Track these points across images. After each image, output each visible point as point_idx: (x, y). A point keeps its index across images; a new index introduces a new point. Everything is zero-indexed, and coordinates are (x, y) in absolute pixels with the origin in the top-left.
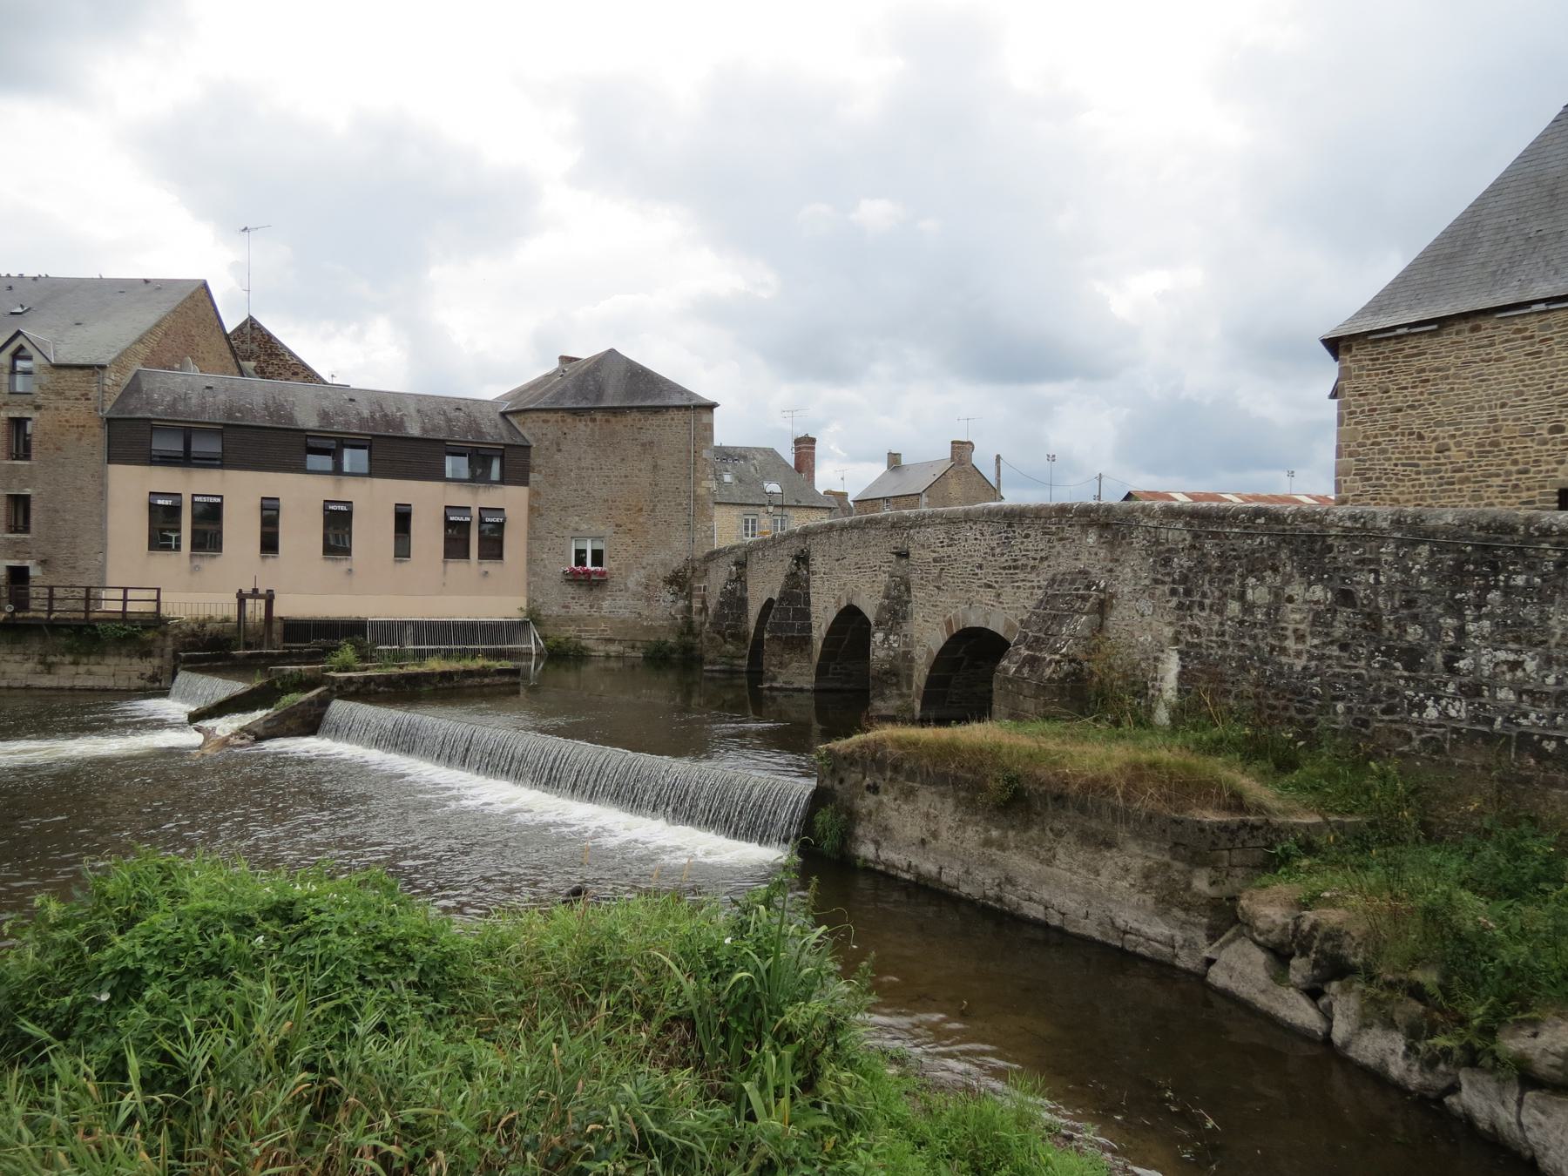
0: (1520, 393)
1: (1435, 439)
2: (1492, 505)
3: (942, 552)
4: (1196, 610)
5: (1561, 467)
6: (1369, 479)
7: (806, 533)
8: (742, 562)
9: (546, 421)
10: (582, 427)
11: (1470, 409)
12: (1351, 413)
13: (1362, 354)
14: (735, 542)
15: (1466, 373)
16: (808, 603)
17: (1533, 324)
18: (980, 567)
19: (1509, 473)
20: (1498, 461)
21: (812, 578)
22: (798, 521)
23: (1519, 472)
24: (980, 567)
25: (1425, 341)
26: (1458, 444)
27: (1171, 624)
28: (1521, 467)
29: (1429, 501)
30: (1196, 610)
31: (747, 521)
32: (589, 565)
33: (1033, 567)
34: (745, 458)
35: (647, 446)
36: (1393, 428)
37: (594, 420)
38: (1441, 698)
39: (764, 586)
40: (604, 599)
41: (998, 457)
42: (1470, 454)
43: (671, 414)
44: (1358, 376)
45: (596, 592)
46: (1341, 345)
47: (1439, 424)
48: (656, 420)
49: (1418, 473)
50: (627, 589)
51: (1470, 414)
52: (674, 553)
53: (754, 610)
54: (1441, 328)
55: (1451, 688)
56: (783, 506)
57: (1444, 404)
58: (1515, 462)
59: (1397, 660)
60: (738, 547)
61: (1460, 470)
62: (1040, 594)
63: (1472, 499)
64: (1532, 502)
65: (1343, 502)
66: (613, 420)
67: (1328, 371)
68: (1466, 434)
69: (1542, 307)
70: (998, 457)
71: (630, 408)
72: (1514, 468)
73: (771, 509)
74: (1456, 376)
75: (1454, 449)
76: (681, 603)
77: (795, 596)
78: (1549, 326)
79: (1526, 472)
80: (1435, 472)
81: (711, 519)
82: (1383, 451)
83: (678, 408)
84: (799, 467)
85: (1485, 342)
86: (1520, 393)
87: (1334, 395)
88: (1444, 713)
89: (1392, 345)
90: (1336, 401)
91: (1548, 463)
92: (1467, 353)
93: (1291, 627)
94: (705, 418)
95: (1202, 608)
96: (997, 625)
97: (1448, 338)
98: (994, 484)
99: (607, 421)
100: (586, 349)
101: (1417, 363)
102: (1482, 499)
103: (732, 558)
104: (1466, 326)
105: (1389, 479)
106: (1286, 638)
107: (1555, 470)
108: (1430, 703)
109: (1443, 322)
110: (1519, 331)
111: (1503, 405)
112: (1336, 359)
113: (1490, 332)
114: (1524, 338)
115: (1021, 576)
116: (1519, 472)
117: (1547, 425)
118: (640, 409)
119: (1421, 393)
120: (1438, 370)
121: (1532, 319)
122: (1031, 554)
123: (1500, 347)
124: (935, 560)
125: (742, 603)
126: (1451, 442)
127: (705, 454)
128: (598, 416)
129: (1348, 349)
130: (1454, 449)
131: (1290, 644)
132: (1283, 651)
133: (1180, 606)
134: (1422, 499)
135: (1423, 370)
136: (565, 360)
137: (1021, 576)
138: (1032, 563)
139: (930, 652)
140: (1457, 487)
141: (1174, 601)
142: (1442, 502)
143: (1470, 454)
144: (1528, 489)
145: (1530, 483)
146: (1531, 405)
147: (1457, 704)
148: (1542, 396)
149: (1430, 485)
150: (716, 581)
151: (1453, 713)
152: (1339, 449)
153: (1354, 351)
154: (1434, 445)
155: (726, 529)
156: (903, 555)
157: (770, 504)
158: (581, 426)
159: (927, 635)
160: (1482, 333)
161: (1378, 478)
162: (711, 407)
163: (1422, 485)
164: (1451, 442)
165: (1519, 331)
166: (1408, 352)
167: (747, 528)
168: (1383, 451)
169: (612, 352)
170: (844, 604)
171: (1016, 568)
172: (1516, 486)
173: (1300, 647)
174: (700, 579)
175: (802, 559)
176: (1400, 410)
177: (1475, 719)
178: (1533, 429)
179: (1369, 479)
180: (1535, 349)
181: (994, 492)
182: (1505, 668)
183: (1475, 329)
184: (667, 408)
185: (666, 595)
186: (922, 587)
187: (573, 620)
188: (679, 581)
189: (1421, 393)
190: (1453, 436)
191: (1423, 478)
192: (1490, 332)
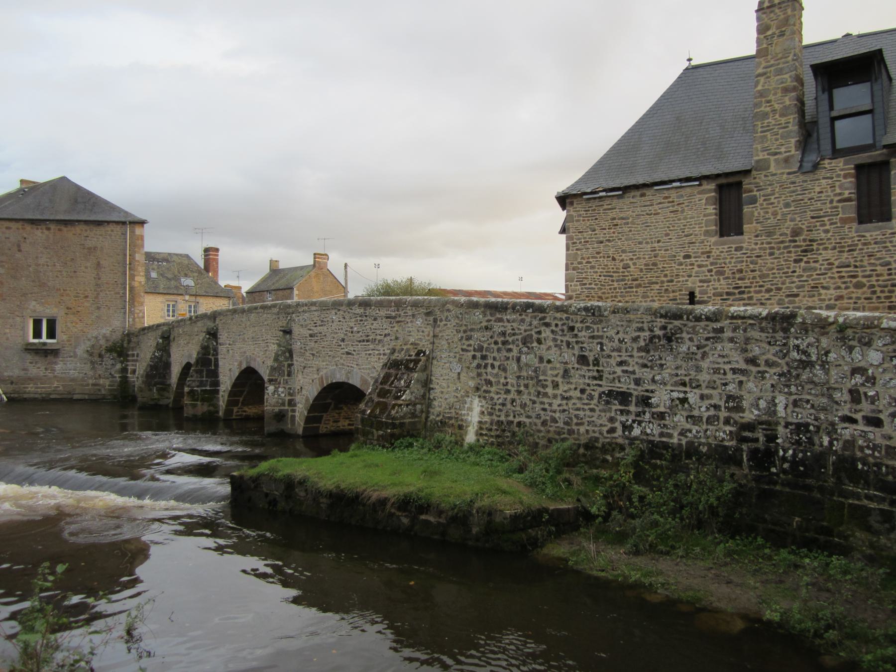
0: (667, 235)
1: (622, 260)
2: (654, 301)
3: (316, 330)
4: (489, 369)
5: (690, 279)
6: (585, 284)
7: (214, 316)
8: (166, 336)
9: (8, 228)
10: (39, 234)
11: (640, 243)
12: (574, 243)
13: (579, 207)
14: (162, 321)
15: (638, 221)
16: (217, 365)
17: (673, 195)
18: (343, 340)
19: (662, 282)
20: (656, 274)
21: (220, 347)
22: (208, 306)
23: (668, 281)
24: (343, 340)
25: (615, 201)
26: (634, 264)
27: (473, 378)
28: (669, 278)
29: (620, 298)
30: (489, 369)
31: (168, 306)
32: (44, 339)
33: (380, 341)
34: (167, 261)
35: (92, 250)
36: (598, 253)
37: (48, 229)
38: (642, 422)
39: (183, 353)
40: (56, 363)
41: (346, 265)
42: (641, 270)
43: (109, 228)
44: (578, 221)
45: (50, 358)
46: (568, 201)
47: (624, 251)
48: (101, 230)
49: (613, 281)
50: (75, 356)
51: (641, 246)
52: (111, 327)
53: (176, 370)
54: (624, 193)
55: (647, 416)
56: (196, 295)
57: (626, 240)
58: (666, 276)
59: (615, 399)
60: (164, 324)
61: (636, 280)
62: (384, 359)
63: (643, 297)
64: (675, 300)
65: (570, 298)
66: (65, 229)
67: (560, 215)
68: (639, 258)
69: (678, 184)
70: (346, 265)
71: (79, 221)
72: (665, 279)
73: (187, 297)
74: (633, 223)
75: (632, 266)
76: (119, 366)
77: (207, 362)
78: (682, 196)
79: (672, 281)
80: (623, 280)
81: (142, 304)
82: (593, 267)
83: (117, 223)
84: (207, 268)
85: (648, 203)
86: (667, 235)
87: (563, 230)
88: (643, 432)
89: (597, 203)
90: (564, 236)
91: (683, 276)
92: (639, 209)
93: (550, 379)
94: (138, 230)
95: (493, 366)
96: (356, 381)
97: (628, 199)
98: (343, 284)
99: (60, 230)
100: (42, 175)
101: (611, 214)
102: (648, 297)
103: (159, 332)
104: (638, 193)
105: (596, 285)
106: (547, 386)
107: (687, 281)
108: (635, 425)
109: (626, 189)
110: (666, 198)
111: (659, 242)
112: (564, 208)
113: (651, 197)
114: (669, 202)
115: (372, 347)
116: (668, 281)
117: (682, 254)
118: (86, 222)
119: (614, 233)
120: (623, 218)
121: (672, 191)
122: (378, 332)
123: (656, 207)
124: (311, 336)
125: (167, 365)
126: (631, 263)
127: (138, 257)
128: (53, 226)
129: (572, 204)
130: (632, 266)
131: (550, 391)
132: (546, 395)
133: (479, 366)
134: (616, 297)
135: (614, 219)
136: (22, 181)
137: (372, 347)
138: (379, 337)
139: (307, 400)
140: (634, 290)
141: (476, 363)
142: (627, 299)
143: (641, 270)
144: (673, 292)
145: (674, 288)
146: (674, 241)
147: (651, 425)
148: (679, 237)
149: (620, 288)
150: (144, 356)
151: (649, 431)
152: (567, 265)
153: (575, 205)
154: (621, 264)
155: (153, 311)
156: (288, 332)
157: (187, 294)
158: (39, 233)
159: (306, 386)
160: (647, 198)
161: (590, 284)
162: (142, 223)
163: (615, 289)
164: (631, 263)
165: (666, 198)
166: (606, 207)
167: (168, 311)
168: (593, 267)
169: (64, 179)
170: (244, 366)
171: (368, 341)
172: (666, 290)
173: (556, 392)
174: (133, 349)
175: (213, 335)
176: (602, 242)
177: (662, 435)
178: (675, 256)
179: (585, 284)
180: (674, 209)
181: (345, 289)
182: (678, 402)
183: (643, 195)
184: (108, 222)
185: (108, 360)
186: (302, 355)
187: (30, 379)
188: (121, 349)
189: (614, 233)
190: (632, 259)
191: (616, 284)
192: (651, 197)
